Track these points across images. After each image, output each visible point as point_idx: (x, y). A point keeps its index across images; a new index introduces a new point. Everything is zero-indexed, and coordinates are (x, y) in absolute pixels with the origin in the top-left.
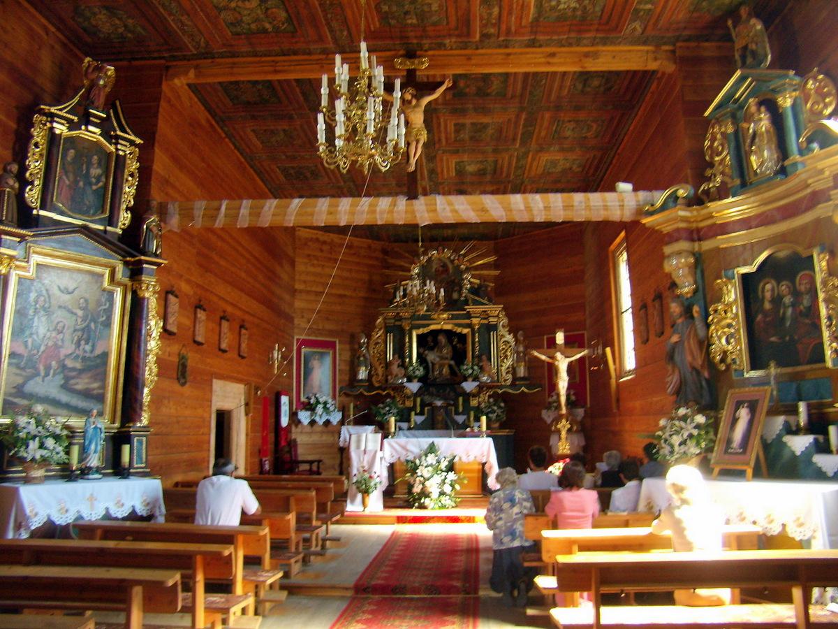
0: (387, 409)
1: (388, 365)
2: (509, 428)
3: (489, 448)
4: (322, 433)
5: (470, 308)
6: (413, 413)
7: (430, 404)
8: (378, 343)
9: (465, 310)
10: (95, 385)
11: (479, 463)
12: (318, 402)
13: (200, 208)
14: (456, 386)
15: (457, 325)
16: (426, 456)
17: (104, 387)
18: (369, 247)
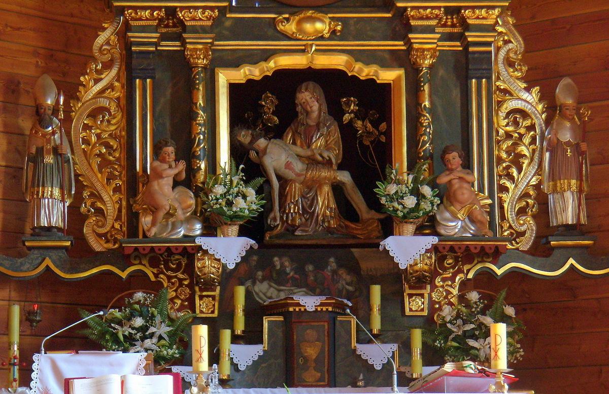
0: (139, 322)
8: (102, 110)
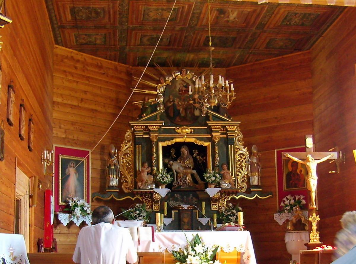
0: (138, 212)
3: (248, 238)
7: (174, 209)
8: (127, 154)
12: (76, 206)
15: (200, 139)
18: (116, 69)
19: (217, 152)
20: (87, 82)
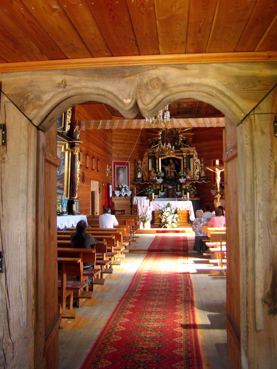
0: (150, 189)
1: (149, 172)
2: (198, 197)
4: (124, 199)
5: (182, 149)
6: (160, 191)
7: (166, 188)
8: (145, 163)
9: (180, 149)
10: (61, 185)
11: (186, 211)
13: (93, 123)
14: (177, 180)
15: (178, 156)
16: (167, 208)
17: (63, 185)
19: (185, 161)
20: (128, 131)
